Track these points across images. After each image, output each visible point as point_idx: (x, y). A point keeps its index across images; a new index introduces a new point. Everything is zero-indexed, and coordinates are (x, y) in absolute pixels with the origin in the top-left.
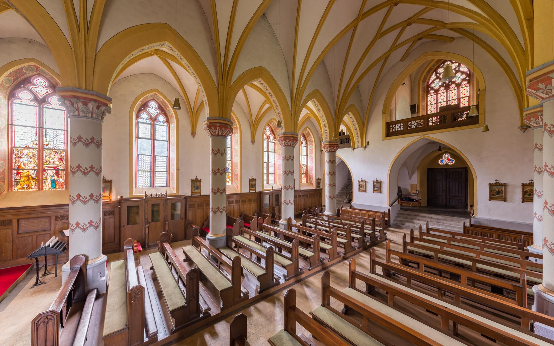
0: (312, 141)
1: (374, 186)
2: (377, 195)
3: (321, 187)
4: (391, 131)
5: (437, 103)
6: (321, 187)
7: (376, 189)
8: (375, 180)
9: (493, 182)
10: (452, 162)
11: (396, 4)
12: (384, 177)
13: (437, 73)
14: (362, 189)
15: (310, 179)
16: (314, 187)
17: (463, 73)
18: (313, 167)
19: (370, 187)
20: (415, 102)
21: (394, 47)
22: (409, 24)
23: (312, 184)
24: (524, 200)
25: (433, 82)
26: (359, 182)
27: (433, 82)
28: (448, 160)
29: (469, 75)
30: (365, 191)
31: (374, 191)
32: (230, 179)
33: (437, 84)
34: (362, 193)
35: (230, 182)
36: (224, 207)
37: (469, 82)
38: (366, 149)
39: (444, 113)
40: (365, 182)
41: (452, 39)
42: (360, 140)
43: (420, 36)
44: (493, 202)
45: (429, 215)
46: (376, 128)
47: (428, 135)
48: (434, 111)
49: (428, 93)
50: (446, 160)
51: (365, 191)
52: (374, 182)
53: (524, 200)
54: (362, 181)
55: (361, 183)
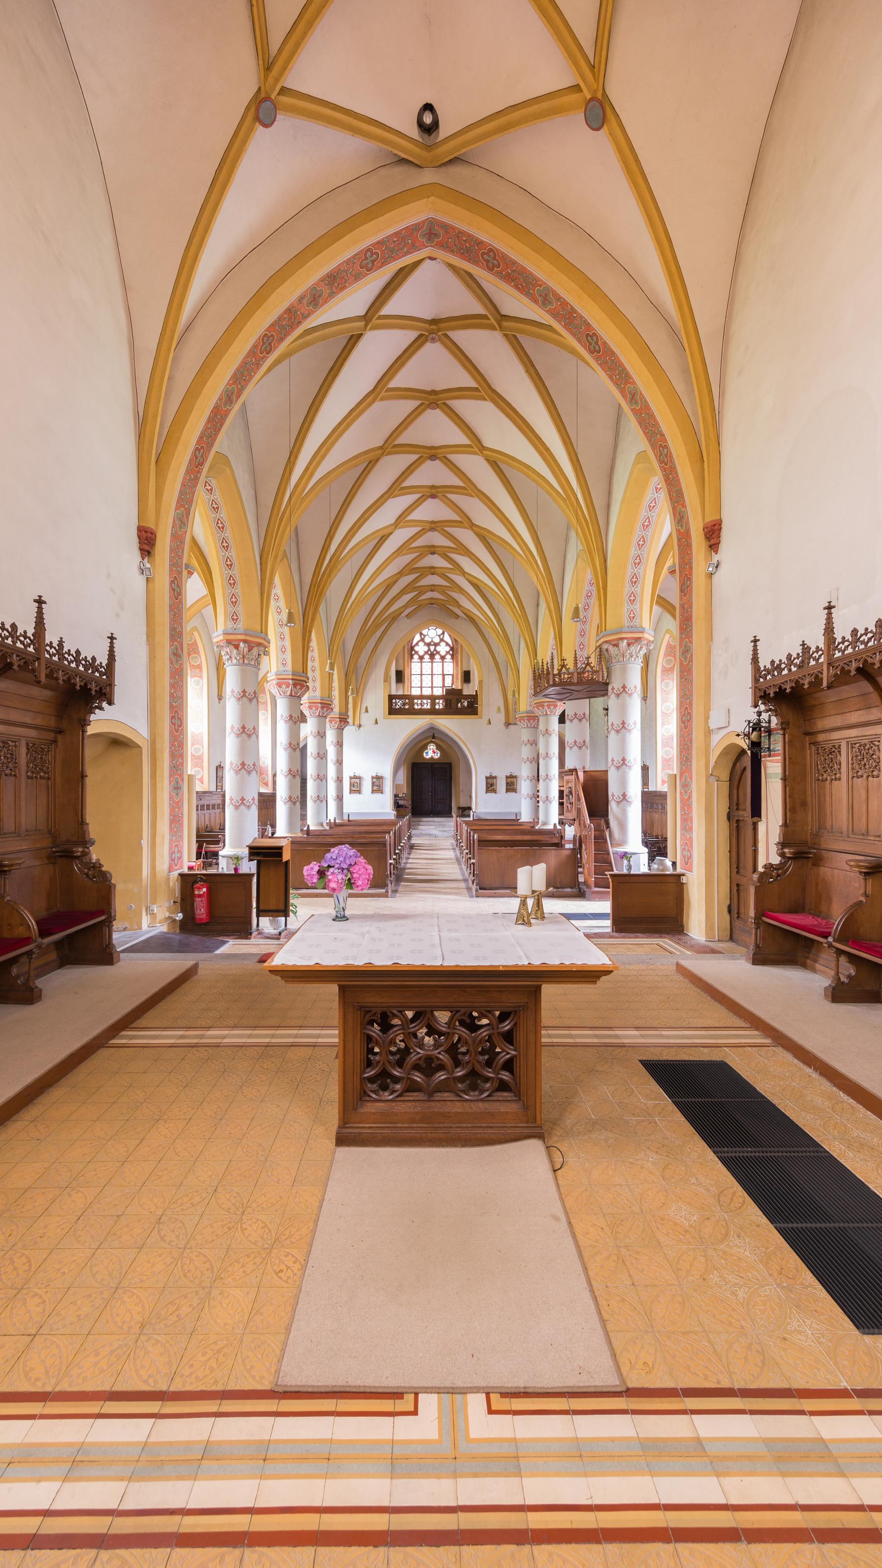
0: (266, 703)
1: (373, 783)
2: (378, 796)
5: (444, 686)
8: (374, 775)
9: (488, 775)
10: (437, 756)
11: (433, 574)
12: (386, 769)
13: (421, 634)
14: (355, 789)
17: (447, 644)
19: (367, 786)
20: (400, 669)
22: (433, 496)
23: (266, 784)
24: (508, 790)
25: (417, 644)
27: (417, 644)
28: (434, 752)
29: (452, 649)
31: (373, 791)
33: (421, 649)
34: (355, 796)
36: (253, 799)
37: (452, 658)
38: (361, 729)
39: (450, 697)
40: (360, 778)
41: (457, 617)
43: (433, 602)
44: (488, 794)
45: (431, 819)
46: (375, 699)
47: (437, 720)
49: (412, 658)
50: (431, 753)
52: (373, 778)
53: (508, 790)
54: (355, 777)
55: (353, 780)
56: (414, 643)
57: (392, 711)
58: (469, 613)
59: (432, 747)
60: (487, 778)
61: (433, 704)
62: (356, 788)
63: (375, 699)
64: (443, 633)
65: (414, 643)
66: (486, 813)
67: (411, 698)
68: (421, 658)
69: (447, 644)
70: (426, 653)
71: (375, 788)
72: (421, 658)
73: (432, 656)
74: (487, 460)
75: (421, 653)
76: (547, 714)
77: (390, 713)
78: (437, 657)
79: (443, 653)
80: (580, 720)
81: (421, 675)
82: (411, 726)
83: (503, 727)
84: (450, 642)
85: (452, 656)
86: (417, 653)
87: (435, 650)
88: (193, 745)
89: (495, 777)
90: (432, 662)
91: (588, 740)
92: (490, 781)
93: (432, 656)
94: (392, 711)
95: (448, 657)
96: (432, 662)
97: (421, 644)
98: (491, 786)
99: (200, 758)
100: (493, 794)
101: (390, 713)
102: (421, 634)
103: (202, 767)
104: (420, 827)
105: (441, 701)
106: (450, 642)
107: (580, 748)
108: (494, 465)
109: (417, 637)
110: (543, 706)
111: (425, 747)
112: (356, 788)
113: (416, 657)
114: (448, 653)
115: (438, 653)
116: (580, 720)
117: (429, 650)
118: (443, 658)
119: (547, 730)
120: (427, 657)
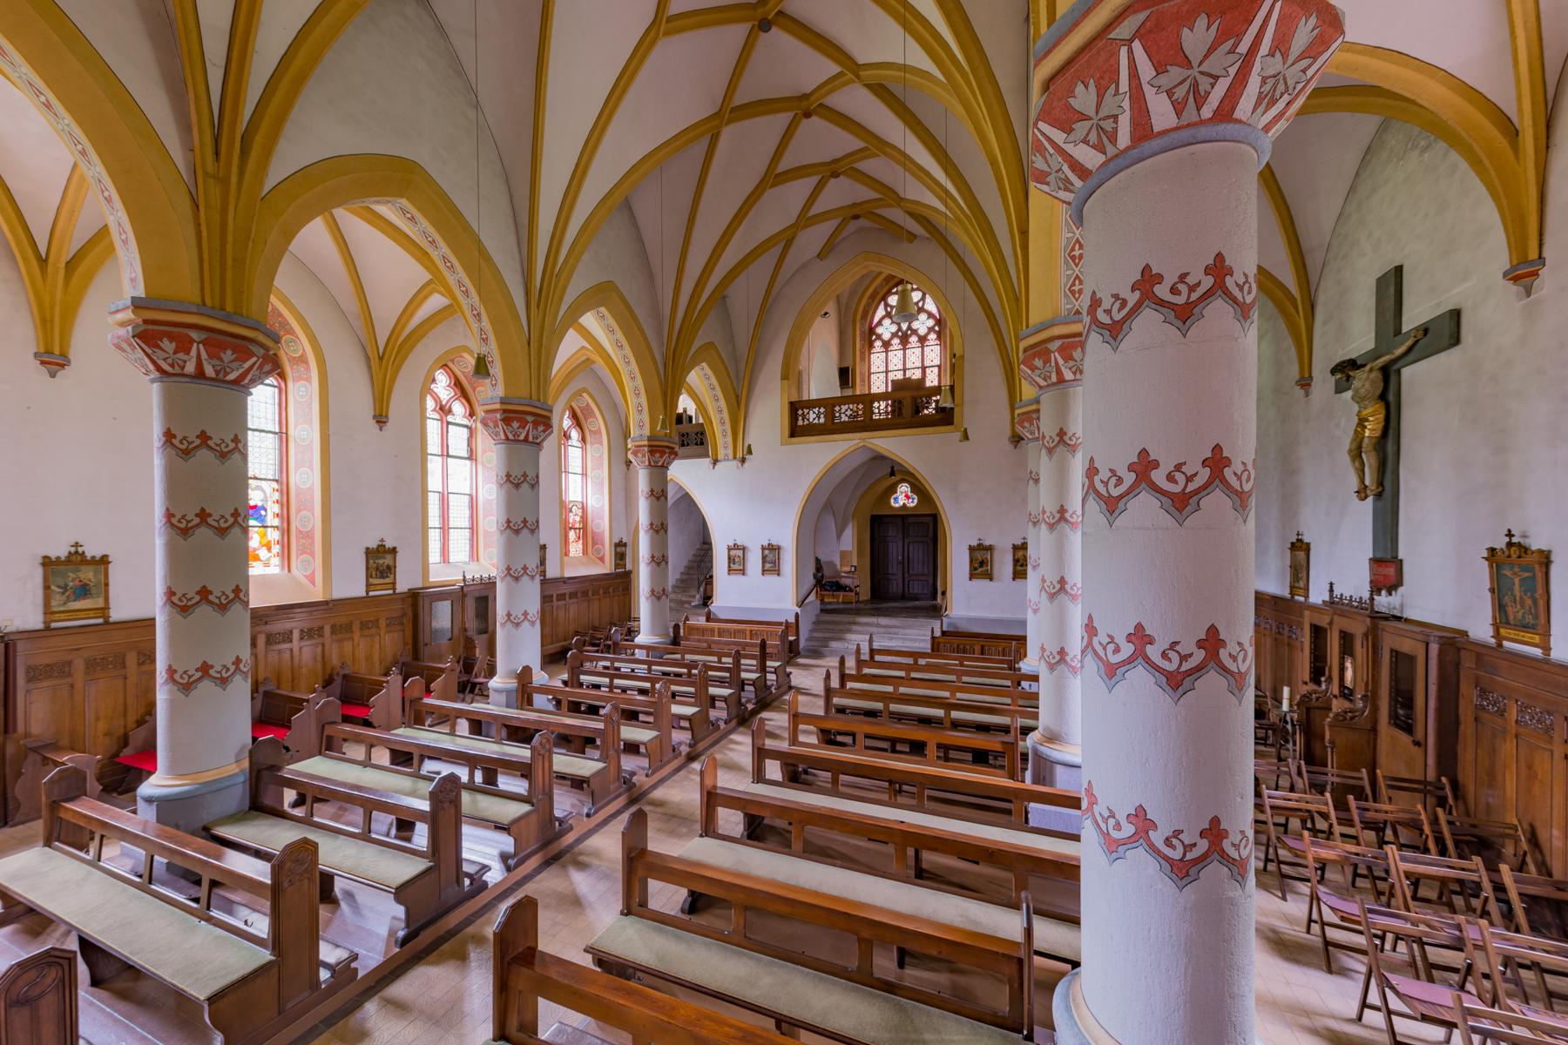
3: (629, 567)
4: (800, 423)
6: (629, 567)
7: (768, 566)
9: (975, 543)
10: (912, 503)
11: (808, 115)
13: (887, 305)
14: (735, 567)
15: (594, 544)
16: (606, 568)
17: (930, 315)
18: (602, 508)
19: (754, 561)
21: (805, 220)
23: (602, 559)
26: (729, 549)
27: (880, 323)
28: (907, 497)
29: (939, 322)
30: (743, 572)
32: (276, 549)
34: (738, 578)
35: (276, 561)
37: (939, 338)
39: (899, 395)
40: (744, 549)
41: (912, 237)
42: (729, 439)
43: (856, 211)
44: (976, 582)
46: (768, 415)
48: (882, 389)
49: (871, 346)
50: (903, 498)
51: (743, 572)
52: (763, 548)
54: (736, 547)
56: (876, 320)
57: (795, 431)
58: (919, 210)
59: (904, 488)
60: (971, 549)
61: (831, 415)
62: (737, 564)
63: (768, 415)
64: (923, 299)
65: (876, 320)
66: (969, 619)
67: (869, 399)
68: (887, 344)
69: (930, 315)
70: (894, 335)
71: (768, 566)
72: (887, 344)
73: (904, 340)
74: (869, 86)
75: (886, 336)
76: (1061, 380)
77: (792, 435)
78: (914, 339)
79: (922, 331)
80: (1184, 315)
81: (887, 372)
82: (823, 454)
83: (1008, 447)
84: (934, 310)
85: (939, 336)
86: (879, 337)
87: (909, 328)
88: (298, 511)
89: (990, 548)
90: (904, 349)
91: (1244, 450)
92: (979, 555)
93: (904, 340)
94: (795, 431)
95: (933, 336)
96: (904, 349)
97: (887, 322)
98: (981, 564)
99: (309, 535)
100: (986, 582)
101: (792, 435)
102: (887, 305)
103: (312, 554)
104: (849, 636)
105: (883, 404)
106: (934, 310)
107: (1181, 503)
108: (881, 91)
109: (881, 312)
110: (1045, 355)
111: (892, 489)
112: (737, 564)
113: (878, 344)
114: (931, 330)
115: (915, 332)
116: (1184, 315)
117: (900, 329)
118: (923, 340)
119: (1062, 433)
120: (896, 341)
